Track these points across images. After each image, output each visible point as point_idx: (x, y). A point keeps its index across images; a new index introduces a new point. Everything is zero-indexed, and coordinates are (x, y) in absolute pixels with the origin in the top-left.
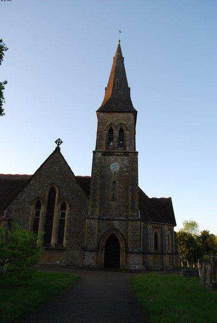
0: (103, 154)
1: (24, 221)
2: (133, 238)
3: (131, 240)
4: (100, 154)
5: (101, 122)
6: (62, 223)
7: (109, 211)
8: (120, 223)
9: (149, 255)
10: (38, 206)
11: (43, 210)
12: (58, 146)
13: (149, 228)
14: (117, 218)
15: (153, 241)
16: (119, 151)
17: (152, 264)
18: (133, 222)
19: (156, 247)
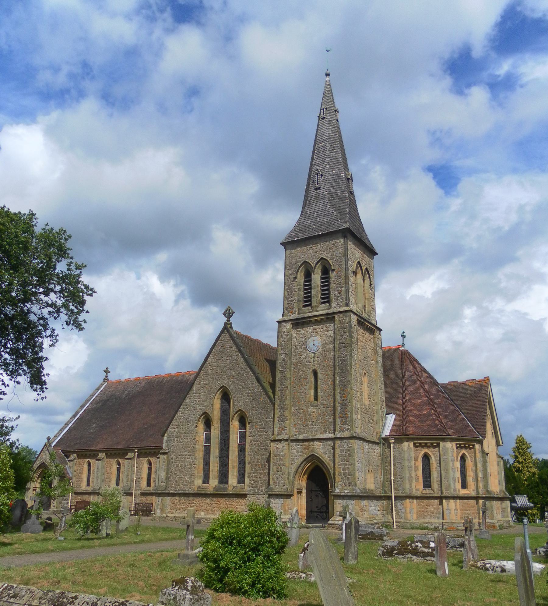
0: (292, 324)
1: (189, 452)
2: (344, 469)
3: (340, 474)
4: (288, 326)
5: (290, 263)
6: (242, 449)
7: (307, 425)
8: (324, 445)
9: (408, 501)
10: (208, 424)
11: (215, 431)
12: (228, 320)
13: (406, 449)
14: (322, 436)
15: (458, 475)
16: (317, 313)
17: (415, 516)
18: (344, 442)
19: (427, 484)
